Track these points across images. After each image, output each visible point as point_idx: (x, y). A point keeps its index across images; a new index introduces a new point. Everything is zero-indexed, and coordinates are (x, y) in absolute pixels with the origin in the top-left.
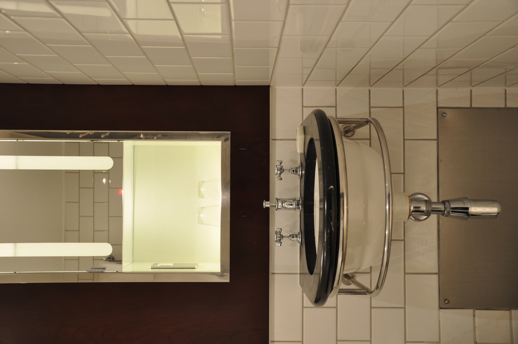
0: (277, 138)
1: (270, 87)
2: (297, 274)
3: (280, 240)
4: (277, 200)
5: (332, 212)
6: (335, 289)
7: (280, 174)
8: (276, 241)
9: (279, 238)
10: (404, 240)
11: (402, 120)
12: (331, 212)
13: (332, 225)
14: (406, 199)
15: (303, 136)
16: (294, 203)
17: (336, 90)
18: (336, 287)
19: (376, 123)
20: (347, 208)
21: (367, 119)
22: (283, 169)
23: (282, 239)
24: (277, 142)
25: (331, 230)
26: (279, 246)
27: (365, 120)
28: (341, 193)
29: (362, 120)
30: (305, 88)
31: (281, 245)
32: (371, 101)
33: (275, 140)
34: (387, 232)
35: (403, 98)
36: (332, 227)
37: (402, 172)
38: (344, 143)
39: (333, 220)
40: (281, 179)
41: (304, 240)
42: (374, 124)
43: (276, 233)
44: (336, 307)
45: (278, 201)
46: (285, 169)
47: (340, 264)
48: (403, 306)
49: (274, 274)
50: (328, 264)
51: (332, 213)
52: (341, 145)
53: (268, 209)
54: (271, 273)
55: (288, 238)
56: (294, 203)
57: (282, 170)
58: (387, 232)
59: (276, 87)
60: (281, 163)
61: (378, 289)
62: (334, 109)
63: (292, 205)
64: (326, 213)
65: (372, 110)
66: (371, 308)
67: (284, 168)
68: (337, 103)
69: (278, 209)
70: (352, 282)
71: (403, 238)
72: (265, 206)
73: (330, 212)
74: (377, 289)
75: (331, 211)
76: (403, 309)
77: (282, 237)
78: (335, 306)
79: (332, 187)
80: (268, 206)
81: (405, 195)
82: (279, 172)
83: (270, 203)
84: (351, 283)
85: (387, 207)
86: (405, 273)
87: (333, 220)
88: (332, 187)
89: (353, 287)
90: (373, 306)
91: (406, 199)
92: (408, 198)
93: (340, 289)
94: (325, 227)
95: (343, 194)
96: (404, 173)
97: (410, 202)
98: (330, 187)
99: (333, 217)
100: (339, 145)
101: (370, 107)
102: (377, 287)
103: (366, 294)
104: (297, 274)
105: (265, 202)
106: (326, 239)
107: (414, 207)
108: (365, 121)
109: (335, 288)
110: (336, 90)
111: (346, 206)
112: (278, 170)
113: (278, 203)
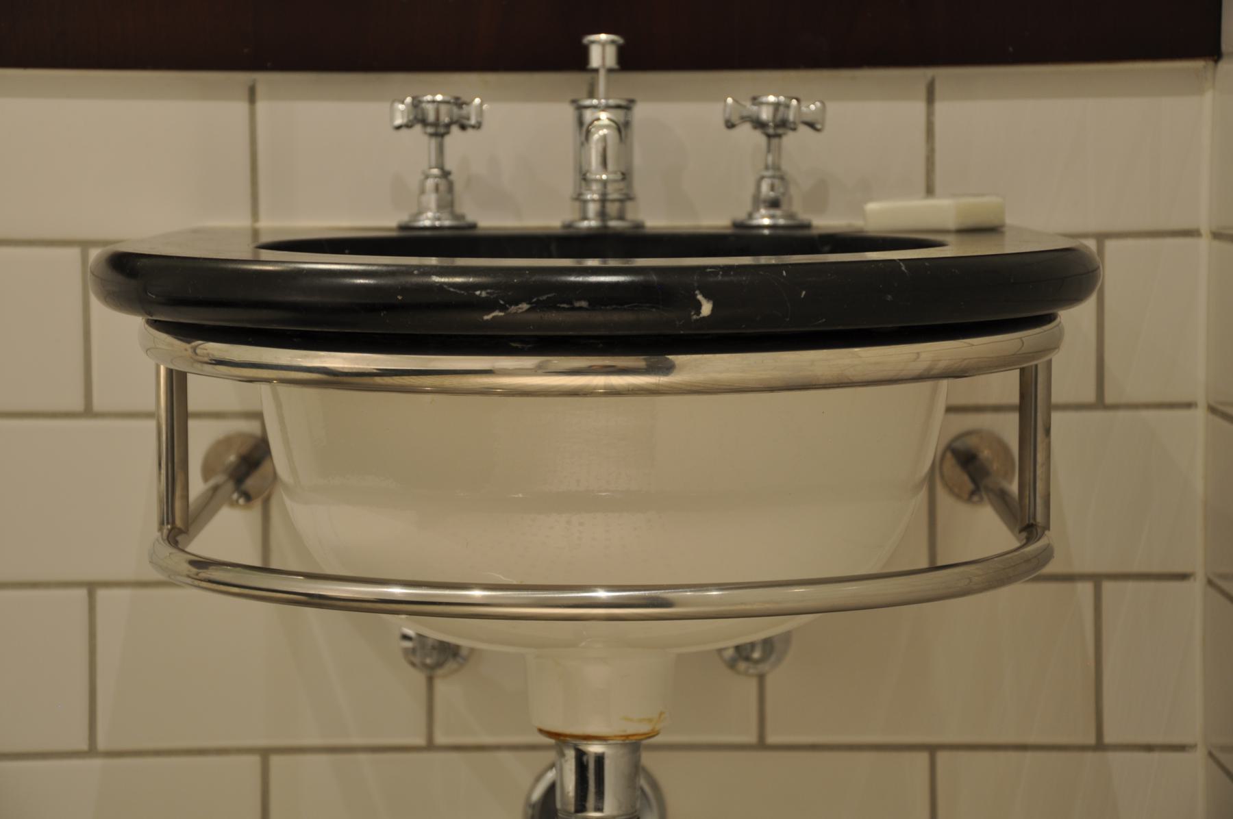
0: (939, 106)
1: (1211, 64)
2: (255, 215)
3: (424, 122)
4: (623, 103)
5: (581, 308)
6: (190, 352)
7: (759, 124)
8: (416, 104)
9: (431, 117)
10: (431, 746)
11: (1032, 739)
12: (577, 304)
13: (513, 309)
14: (641, 721)
15: (951, 224)
16: (612, 177)
17: (1189, 405)
18: (198, 351)
19: (1028, 561)
20: (596, 387)
21: (1048, 528)
22: (779, 136)
23: (430, 130)
24: (920, 107)
25: (489, 305)
26: (392, 119)
27: (1040, 519)
28: (671, 361)
29: (1039, 501)
30: (1204, 244)
31: (399, 128)
32: (1131, 585)
33: (930, 99)
34: (477, 594)
35: (1149, 748)
36: (503, 308)
37: (772, 739)
38: (926, 386)
39: (535, 316)
40: (730, 125)
41: (427, 233)
42: (1022, 551)
43: (459, 103)
44: (88, 412)
45: (618, 107)
46: (780, 147)
47: (316, 363)
48: (102, 744)
49: (252, 97)
50: (316, 299)
51: (573, 309)
52: (919, 367)
53: (578, 61)
54: (254, 82)
55: (433, 163)
56: (615, 173)
57: (776, 128)
58: (477, 594)
59: (1209, 96)
60: (811, 125)
61: (194, 570)
62: (1090, 396)
63: (604, 163)
64: (573, 279)
65: (1086, 588)
66: (92, 587)
67: (791, 135)
68: (1121, 414)
69: (580, 108)
70: (215, 489)
71: (440, 739)
72: (593, 42)
73: (580, 299)
74: (192, 563)
75: (584, 304)
76: (84, 746)
77: (439, 131)
78: (98, 405)
79: (707, 309)
80: (595, 59)
81: (661, 714)
82: (766, 114)
83: (610, 71)
84: (212, 482)
85: (602, 594)
86: (265, 753)
87: (535, 316)
88: (707, 309)
89: (197, 486)
90: (101, 594)
91: (641, 721)
92: (644, 728)
93: (183, 376)
94: (501, 279)
95: (668, 369)
96: (762, 745)
97: (627, 736)
98: (707, 297)
99: (553, 316)
100: (915, 360)
101: (1097, 579)
102: (201, 563)
103: (162, 523)
104: (255, 215)
105: (613, 42)
106: (442, 285)
107: (600, 759)
108: (1035, 518)
109: (194, 349)
110: (1189, 405)
111: (605, 387)
112: (777, 106)
113: (607, 108)
